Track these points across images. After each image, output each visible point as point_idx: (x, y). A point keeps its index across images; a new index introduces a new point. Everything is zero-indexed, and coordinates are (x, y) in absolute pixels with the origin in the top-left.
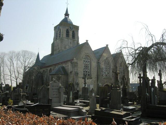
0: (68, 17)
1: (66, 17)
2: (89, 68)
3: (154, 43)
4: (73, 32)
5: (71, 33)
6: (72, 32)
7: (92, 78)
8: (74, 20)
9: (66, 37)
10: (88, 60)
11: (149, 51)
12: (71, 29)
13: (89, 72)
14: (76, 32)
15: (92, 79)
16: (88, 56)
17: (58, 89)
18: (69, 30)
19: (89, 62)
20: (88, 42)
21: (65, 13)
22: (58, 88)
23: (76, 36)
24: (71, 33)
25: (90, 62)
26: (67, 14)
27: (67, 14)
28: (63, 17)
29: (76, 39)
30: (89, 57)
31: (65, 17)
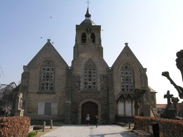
2: (132, 81)
3: (17, 86)
5: (88, 36)
7: (55, 93)
8: (95, 21)
9: (81, 43)
10: (51, 68)
11: (134, 125)
12: (88, 31)
13: (131, 87)
14: (96, 34)
15: (55, 95)
16: (51, 61)
17: (29, 93)
18: (86, 34)
19: (131, 73)
20: (128, 45)
21: (86, 14)
22: (29, 94)
23: (96, 39)
24: (88, 36)
25: (133, 74)
26: (88, 15)
27: (88, 15)
28: (84, 18)
29: (97, 42)
30: (52, 62)
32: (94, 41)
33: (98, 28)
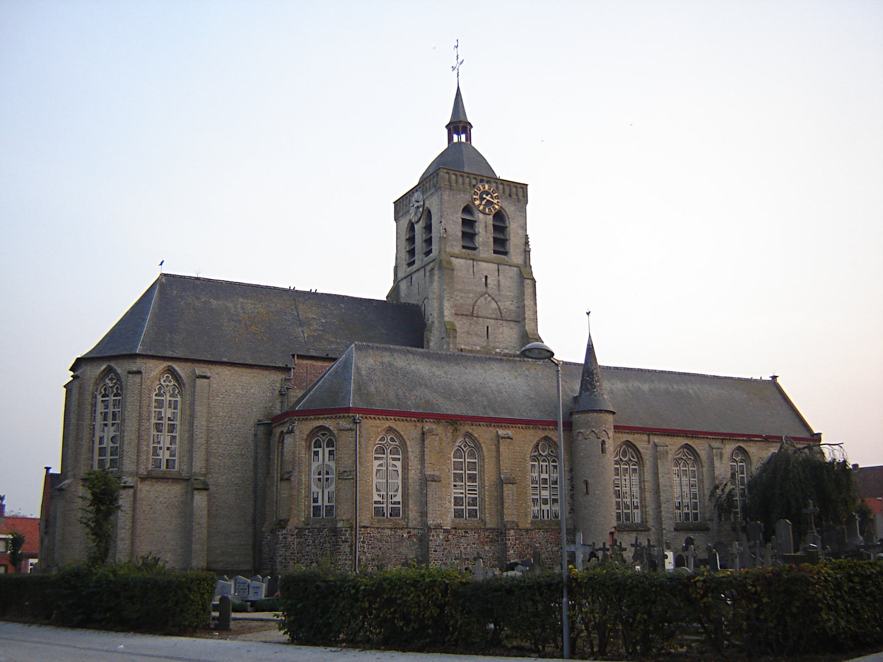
0: (469, 138)
1: (455, 138)
4: (499, 216)
6: (491, 217)
23: (514, 242)
26: (459, 125)
27: (459, 125)
29: (515, 257)
31: (450, 139)
32: (501, 244)
33: (518, 192)
